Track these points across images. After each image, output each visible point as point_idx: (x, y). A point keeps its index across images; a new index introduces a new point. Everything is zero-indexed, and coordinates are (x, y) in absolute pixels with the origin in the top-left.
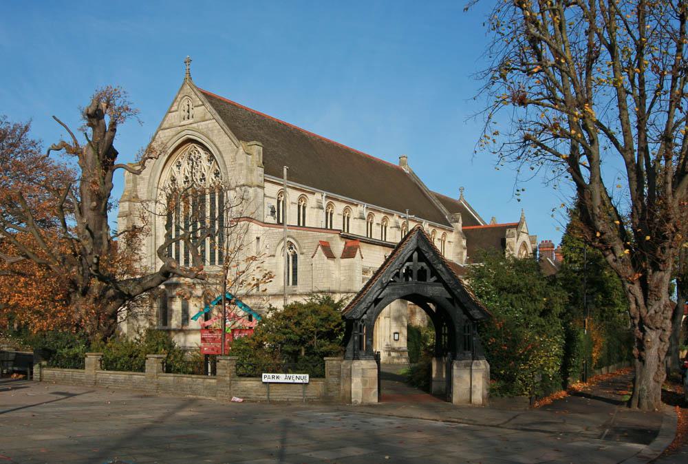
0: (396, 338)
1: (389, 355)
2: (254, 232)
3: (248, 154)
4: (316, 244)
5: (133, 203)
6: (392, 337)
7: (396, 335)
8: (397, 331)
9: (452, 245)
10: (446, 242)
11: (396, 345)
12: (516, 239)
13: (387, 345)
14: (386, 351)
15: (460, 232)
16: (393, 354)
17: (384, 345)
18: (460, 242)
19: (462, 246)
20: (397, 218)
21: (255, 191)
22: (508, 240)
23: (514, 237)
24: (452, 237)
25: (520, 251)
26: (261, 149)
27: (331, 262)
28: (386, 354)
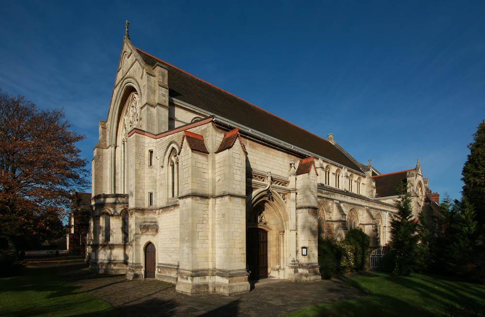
0: (304, 253)
1: (296, 271)
2: (146, 145)
3: (150, 74)
4: (181, 138)
5: (101, 149)
6: (300, 252)
7: (304, 250)
8: (306, 245)
9: (365, 186)
10: (361, 184)
11: (303, 260)
12: (415, 178)
13: (294, 261)
14: (292, 267)
15: (370, 177)
16: (300, 271)
17: (290, 261)
18: (371, 183)
19: (372, 186)
20: (322, 162)
21: (158, 109)
22: (408, 179)
23: (413, 176)
24: (365, 181)
25: (417, 188)
26: (166, 72)
27: (200, 157)
28: (292, 270)
